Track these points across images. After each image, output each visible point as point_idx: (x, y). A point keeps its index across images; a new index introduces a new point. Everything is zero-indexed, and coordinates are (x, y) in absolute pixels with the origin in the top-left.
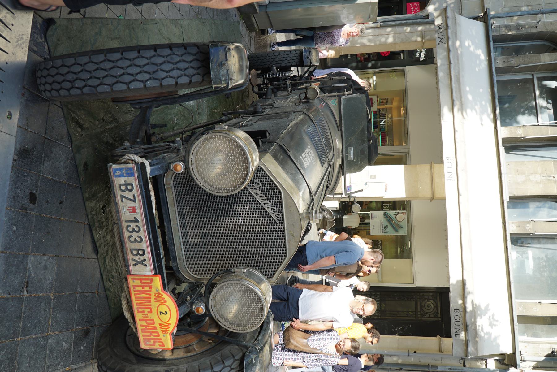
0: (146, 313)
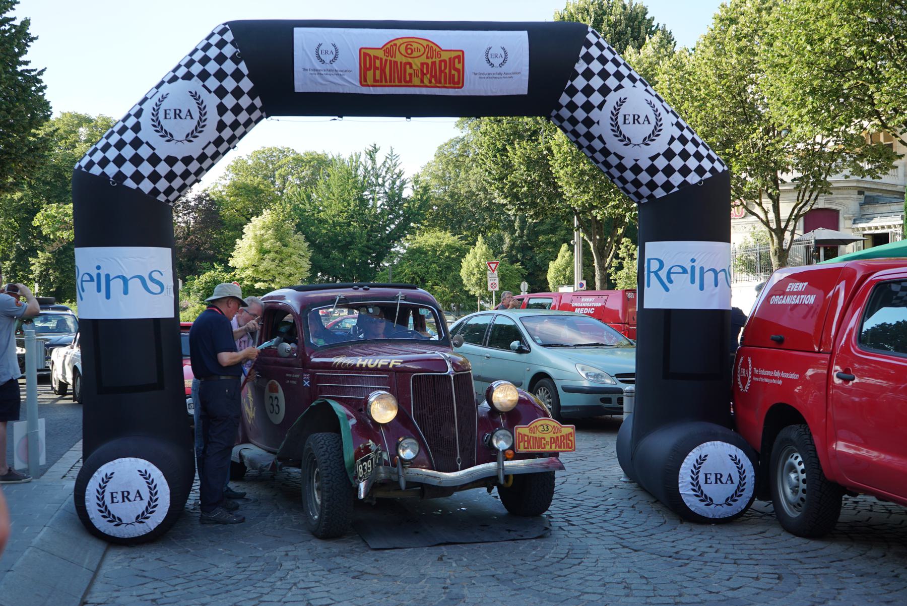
0: (411, 71)
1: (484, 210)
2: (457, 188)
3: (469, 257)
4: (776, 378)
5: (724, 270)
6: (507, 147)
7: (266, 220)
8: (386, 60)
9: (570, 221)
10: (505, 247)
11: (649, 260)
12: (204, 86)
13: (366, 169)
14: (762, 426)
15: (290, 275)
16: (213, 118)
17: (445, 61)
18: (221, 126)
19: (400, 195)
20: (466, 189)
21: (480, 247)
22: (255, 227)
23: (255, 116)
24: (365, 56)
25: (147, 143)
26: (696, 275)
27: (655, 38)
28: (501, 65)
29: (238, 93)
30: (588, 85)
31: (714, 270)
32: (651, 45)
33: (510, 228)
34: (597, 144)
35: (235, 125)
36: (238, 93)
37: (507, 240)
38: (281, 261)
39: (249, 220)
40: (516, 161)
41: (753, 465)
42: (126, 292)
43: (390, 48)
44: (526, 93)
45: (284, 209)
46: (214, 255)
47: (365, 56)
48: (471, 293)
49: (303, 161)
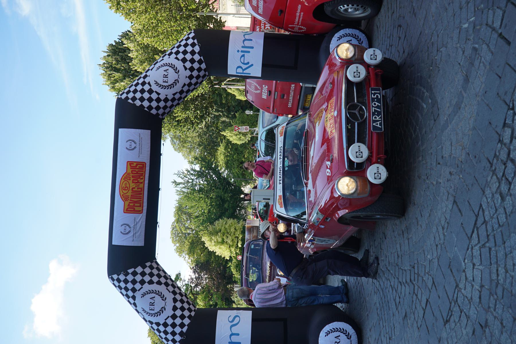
0: (136, 188)
1: (208, 130)
2: (196, 143)
3: (231, 139)
4: (300, 15)
5: (244, 35)
6: (177, 119)
7: (207, 239)
9: (216, 89)
10: (227, 120)
11: (237, 73)
12: (139, 290)
13: (184, 188)
14: (324, 23)
15: (235, 229)
16: (155, 287)
17: (132, 171)
18: (159, 283)
19: (198, 171)
20: (197, 138)
21: (227, 133)
22: (210, 245)
23: (155, 266)
24: (127, 210)
25: (166, 320)
26: (245, 51)
27: (125, 42)
28: (135, 143)
29: (143, 274)
30: (147, 100)
31: (244, 41)
32: (128, 44)
33: (218, 117)
34: (177, 96)
35: (159, 276)
36: (143, 274)
37: (224, 119)
38: (228, 233)
39: (207, 248)
40: (184, 116)
41: (343, 29)
42: (238, 335)
43: (124, 198)
44: (150, 131)
45: (202, 230)
46: (223, 266)
47: (127, 210)
48: (249, 139)
49: (178, 219)
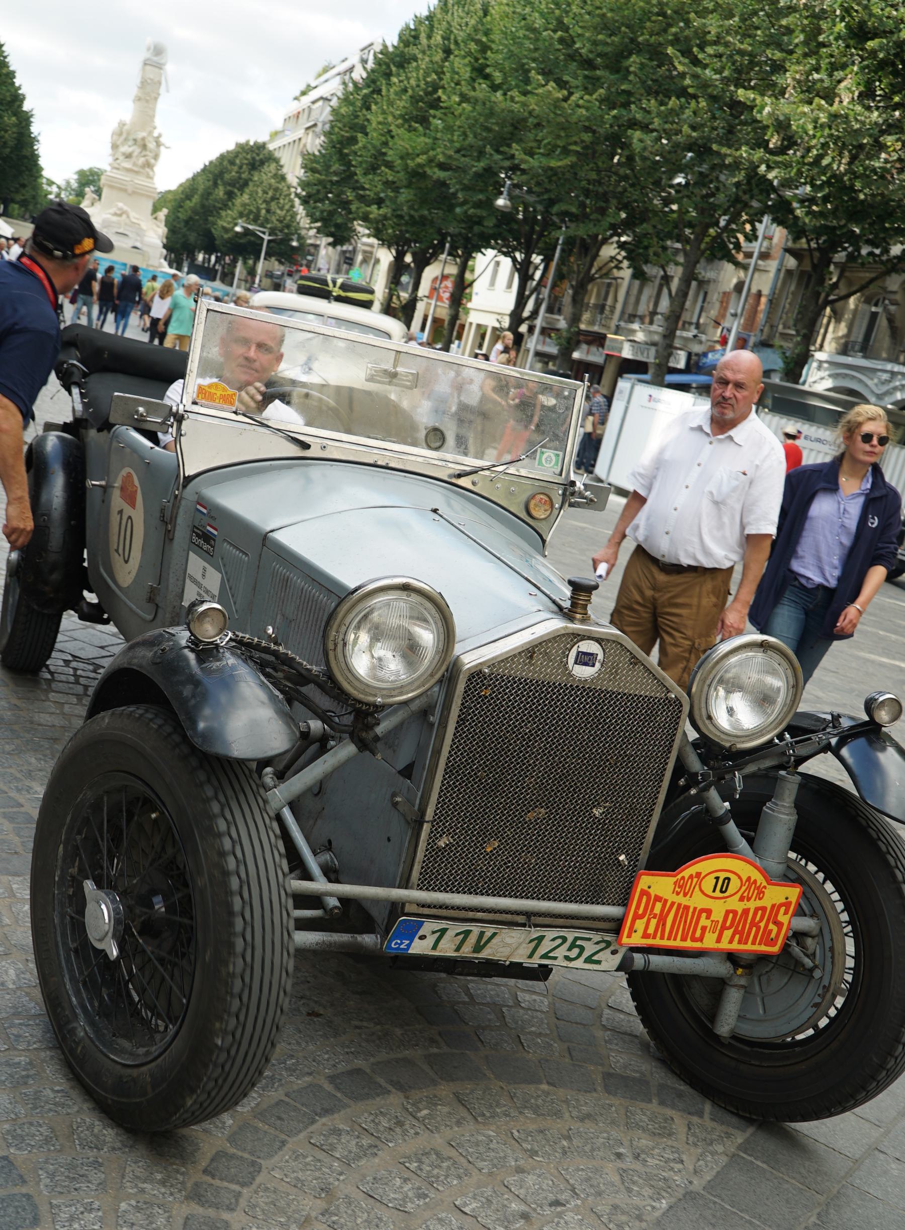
0: (708, 923)
8: (673, 904)
